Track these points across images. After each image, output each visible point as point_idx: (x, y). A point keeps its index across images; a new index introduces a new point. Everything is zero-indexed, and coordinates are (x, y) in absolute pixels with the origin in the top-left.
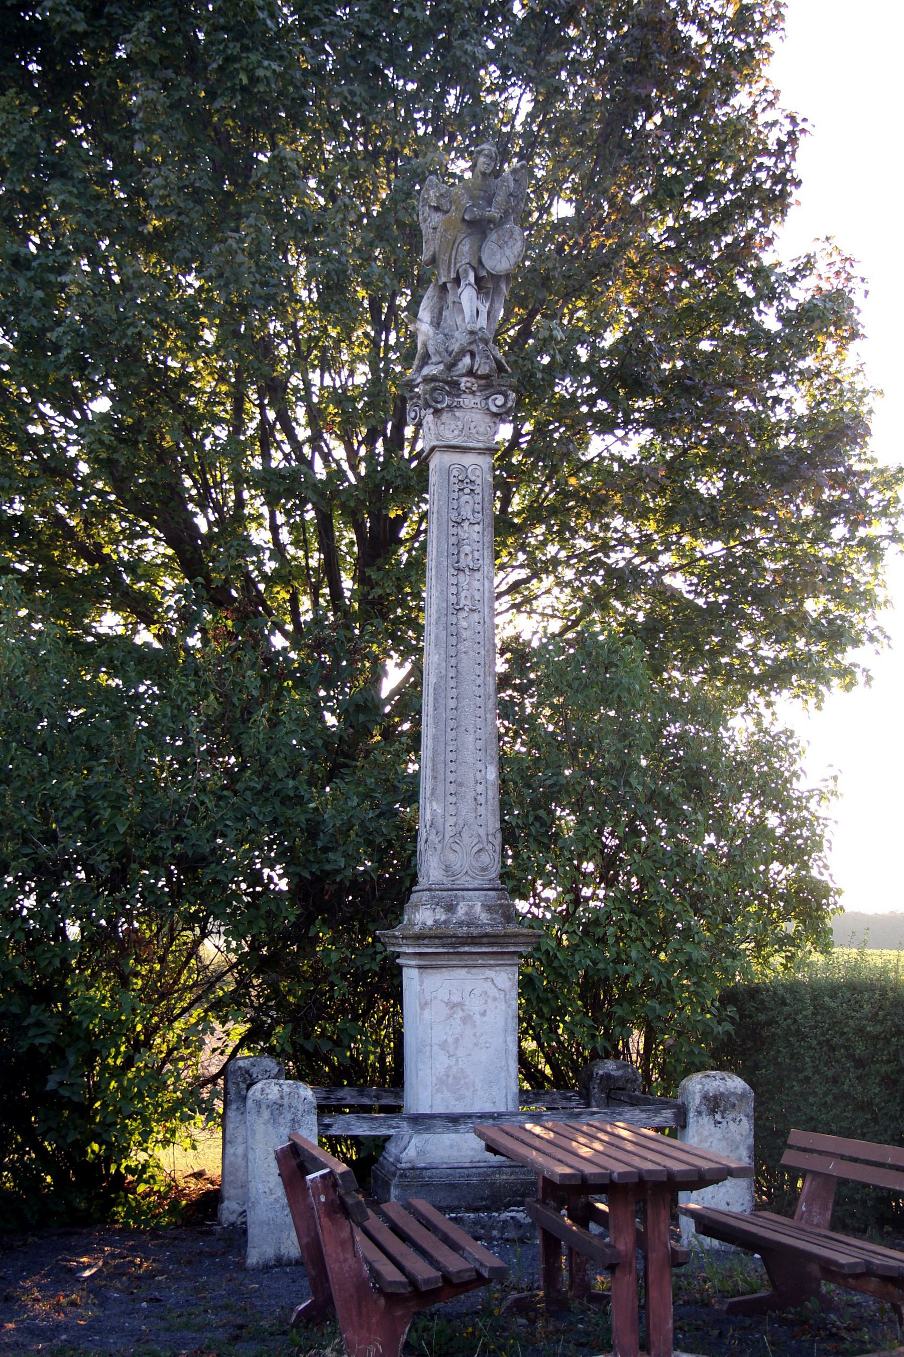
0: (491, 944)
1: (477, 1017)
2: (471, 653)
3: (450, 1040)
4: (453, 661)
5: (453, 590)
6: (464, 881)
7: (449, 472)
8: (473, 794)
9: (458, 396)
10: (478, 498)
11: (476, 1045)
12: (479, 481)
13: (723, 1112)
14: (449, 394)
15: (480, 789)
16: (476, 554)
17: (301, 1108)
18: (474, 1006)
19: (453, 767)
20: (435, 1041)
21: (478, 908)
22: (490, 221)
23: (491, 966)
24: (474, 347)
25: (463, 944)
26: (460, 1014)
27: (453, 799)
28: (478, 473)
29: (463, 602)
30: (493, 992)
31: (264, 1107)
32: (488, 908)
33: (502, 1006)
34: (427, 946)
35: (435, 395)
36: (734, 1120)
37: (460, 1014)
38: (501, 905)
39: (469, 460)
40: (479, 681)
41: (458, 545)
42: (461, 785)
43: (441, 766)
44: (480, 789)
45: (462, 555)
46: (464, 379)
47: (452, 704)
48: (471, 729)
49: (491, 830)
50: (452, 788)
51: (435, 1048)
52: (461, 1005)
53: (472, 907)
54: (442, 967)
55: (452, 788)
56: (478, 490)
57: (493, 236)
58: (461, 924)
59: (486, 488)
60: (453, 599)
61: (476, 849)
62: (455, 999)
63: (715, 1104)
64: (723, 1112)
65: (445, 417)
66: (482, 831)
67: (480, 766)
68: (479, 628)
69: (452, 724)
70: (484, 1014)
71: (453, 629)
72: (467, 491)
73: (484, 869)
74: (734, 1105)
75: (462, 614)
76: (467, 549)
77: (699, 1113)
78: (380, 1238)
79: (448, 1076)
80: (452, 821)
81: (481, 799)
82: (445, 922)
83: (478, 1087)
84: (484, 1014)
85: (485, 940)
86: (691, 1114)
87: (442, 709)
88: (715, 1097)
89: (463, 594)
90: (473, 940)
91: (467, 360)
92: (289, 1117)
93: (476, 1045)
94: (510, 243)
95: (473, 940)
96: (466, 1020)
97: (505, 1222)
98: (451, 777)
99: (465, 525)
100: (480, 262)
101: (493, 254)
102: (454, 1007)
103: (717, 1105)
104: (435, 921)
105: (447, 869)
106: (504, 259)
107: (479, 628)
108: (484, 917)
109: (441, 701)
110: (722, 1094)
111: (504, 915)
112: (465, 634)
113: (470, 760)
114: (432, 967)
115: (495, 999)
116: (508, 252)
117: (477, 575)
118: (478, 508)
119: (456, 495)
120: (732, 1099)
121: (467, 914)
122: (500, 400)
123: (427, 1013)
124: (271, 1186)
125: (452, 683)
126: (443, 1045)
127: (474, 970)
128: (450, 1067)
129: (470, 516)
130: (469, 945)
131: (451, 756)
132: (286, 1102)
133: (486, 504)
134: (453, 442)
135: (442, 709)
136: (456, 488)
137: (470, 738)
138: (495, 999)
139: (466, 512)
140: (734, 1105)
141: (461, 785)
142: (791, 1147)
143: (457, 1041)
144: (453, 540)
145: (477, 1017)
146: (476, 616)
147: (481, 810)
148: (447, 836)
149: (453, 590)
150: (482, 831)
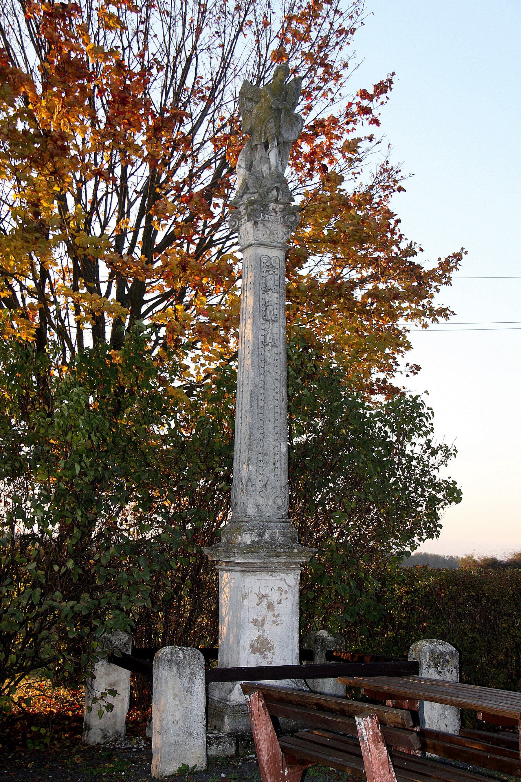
1: (275, 604)
7: (261, 259)
8: (272, 460)
13: (442, 666)
27: (261, 464)
28: (278, 261)
29: (268, 340)
32: (282, 534)
33: (290, 596)
36: (448, 670)
42: (266, 455)
43: (254, 443)
45: (268, 312)
46: (272, 204)
47: (261, 404)
49: (283, 484)
62: (263, 592)
64: (442, 666)
72: (271, 272)
73: (279, 508)
76: (271, 308)
77: (429, 666)
78: (342, 748)
80: (260, 477)
82: (258, 542)
84: (280, 602)
86: (424, 667)
87: (255, 407)
89: (268, 336)
91: (275, 192)
94: (296, 124)
99: (270, 293)
104: (252, 541)
105: (258, 507)
109: (255, 401)
115: (286, 592)
116: (295, 129)
117: (276, 324)
118: (277, 283)
120: (448, 657)
123: (246, 602)
126: (255, 622)
135: (255, 407)
137: (272, 425)
139: (270, 284)
140: (448, 661)
144: (263, 302)
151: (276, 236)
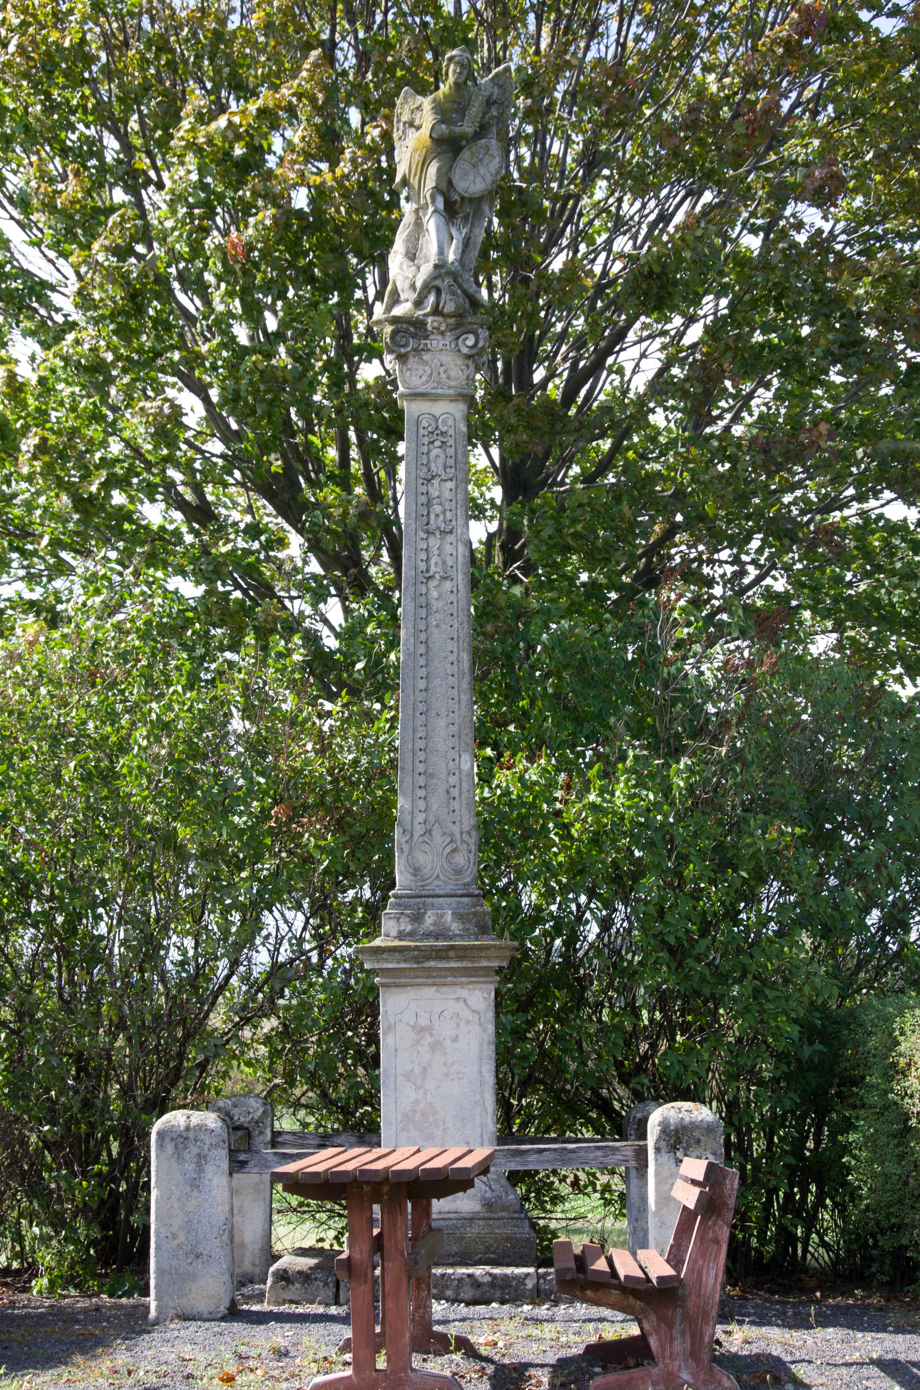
0: (460, 958)
1: (448, 1042)
2: (443, 627)
3: (417, 1070)
4: (423, 637)
5: (423, 556)
6: (437, 886)
8: (443, 787)
9: (426, 338)
10: (451, 451)
11: (447, 1075)
12: (451, 432)
14: (414, 336)
15: (453, 780)
16: (448, 514)
17: (208, 1142)
18: (445, 1030)
19: (422, 756)
20: (400, 1071)
21: (449, 917)
22: (463, 137)
23: (462, 985)
24: (438, 282)
25: (429, 958)
26: (428, 1039)
27: (422, 793)
28: (451, 422)
29: (433, 569)
30: (466, 1014)
31: (167, 1140)
32: (459, 916)
33: (477, 1029)
34: (386, 961)
35: (398, 338)
37: (428, 1039)
38: (475, 914)
39: (440, 408)
40: (453, 658)
41: (428, 504)
42: (432, 776)
44: (453, 780)
45: (432, 517)
46: (430, 319)
47: (422, 684)
48: (443, 712)
50: (421, 781)
51: (400, 1079)
52: (429, 1029)
53: (442, 915)
54: (420, 985)
55: (421, 781)
56: (451, 442)
57: (466, 154)
58: (428, 935)
59: (460, 440)
60: (422, 566)
61: (448, 849)
62: (423, 1021)
63: (678, 1140)
65: (412, 361)
66: (456, 829)
67: (453, 754)
68: (453, 598)
69: (421, 707)
70: (455, 1039)
71: (423, 600)
72: (437, 444)
74: (698, 1141)
75: (433, 583)
76: (437, 509)
79: (415, 1112)
80: (421, 817)
81: (455, 792)
83: (450, 1125)
84: (455, 1039)
85: (451, 954)
88: (677, 1131)
89: (433, 561)
90: (440, 954)
92: (195, 1151)
93: (447, 1075)
94: (486, 160)
95: (440, 954)
96: (436, 1046)
97: (460, 1280)
98: (421, 768)
99: (436, 482)
100: (450, 183)
101: (466, 174)
102: (421, 1031)
103: (678, 1141)
106: (478, 180)
107: (453, 598)
108: (455, 927)
110: (684, 1128)
111: (478, 925)
112: (435, 605)
113: (442, 747)
114: (397, 986)
115: (468, 1022)
117: (450, 538)
118: (451, 462)
119: (425, 449)
120: (697, 1134)
121: (435, 924)
122: (471, 341)
124: (174, 1230)
125: (422, 661)
126: (408, 1076)
127: (444, 989)
128: (417, 1101)
129: (441, 471)
130: (435, 959)
131: (421, 744)
132: (191, 1135)
133: (460, 457)
134: (421, 390)
136: (426, 440)
137: (442, 723)
138: (468, 1022)
141: (432, 776)
142: (694, 1182)
143: (425, 1070)
145: (448, 1042)
146: (448, 585)
147: (456, 805)
148: (416, 835)
149: (423, 556)
150: (456, 829)
151: (444, 376)
